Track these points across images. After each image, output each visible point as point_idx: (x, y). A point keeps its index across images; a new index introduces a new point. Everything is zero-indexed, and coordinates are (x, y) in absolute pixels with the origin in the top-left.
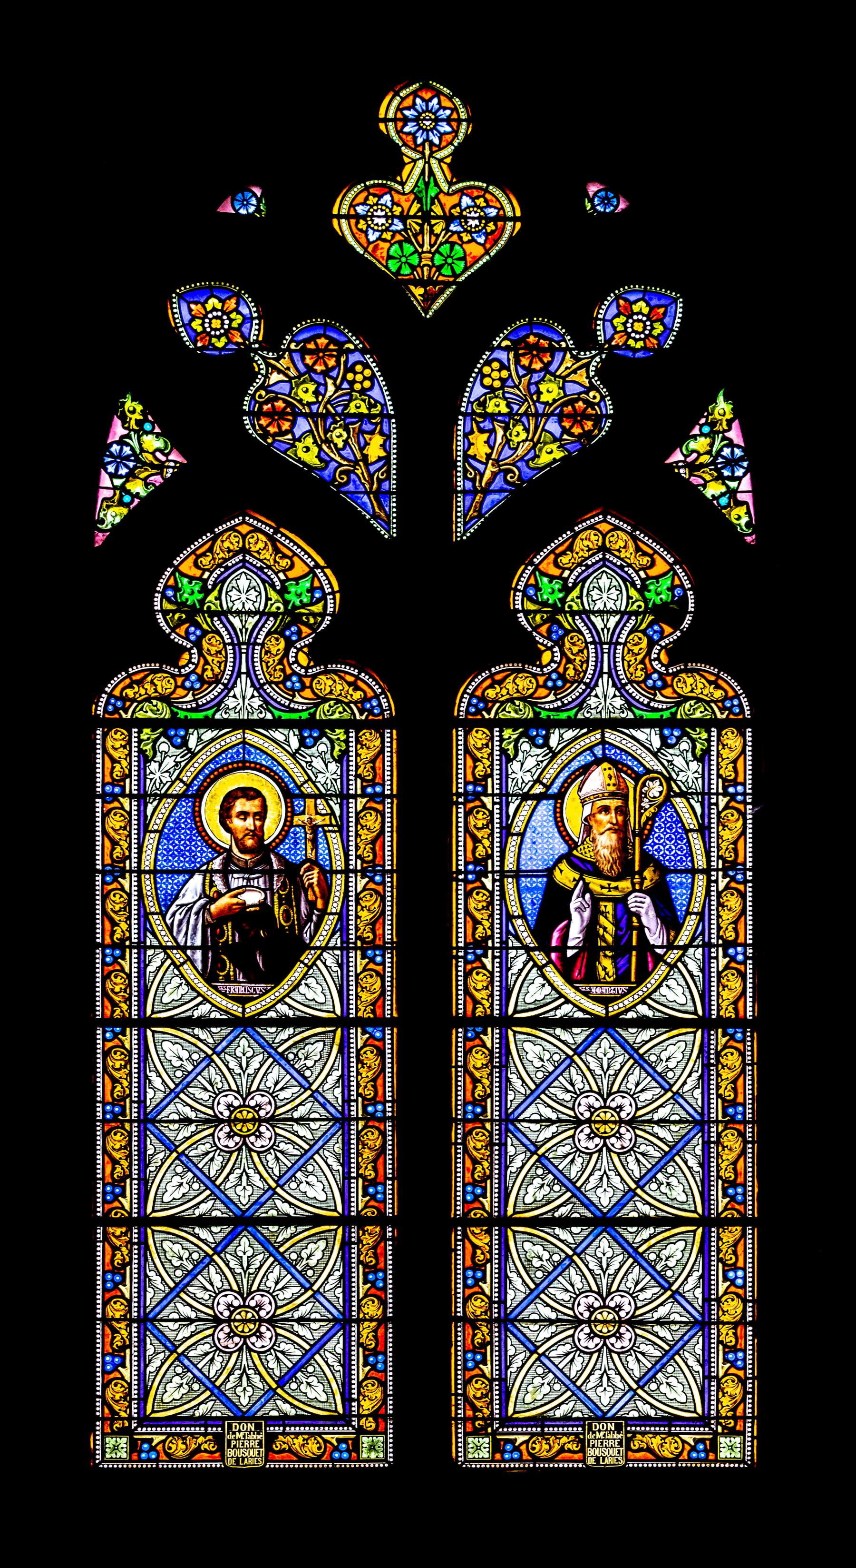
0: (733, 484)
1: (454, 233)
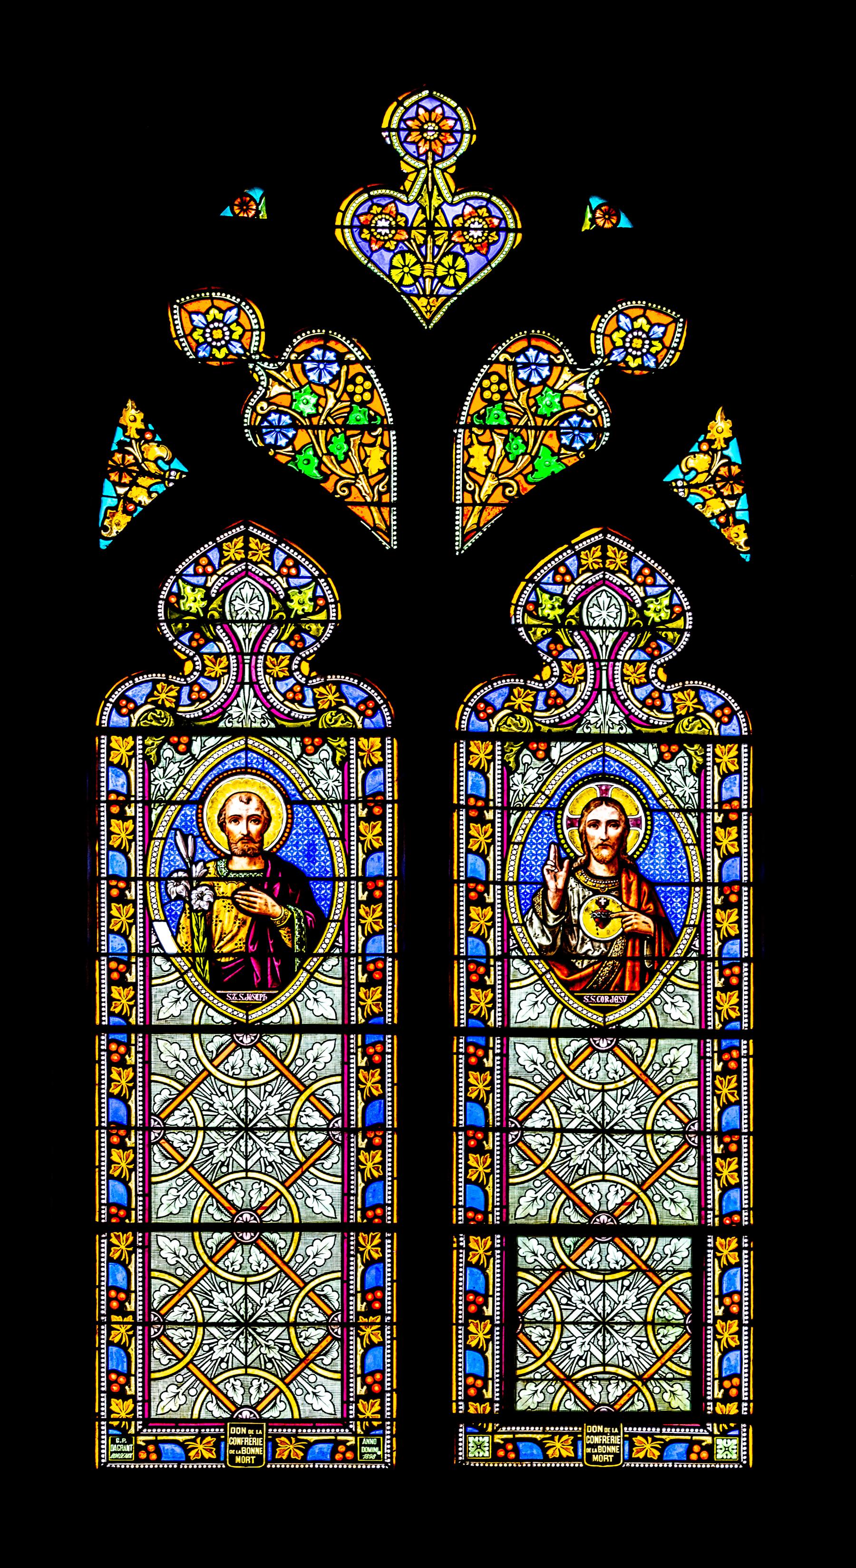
1: (456, 243)
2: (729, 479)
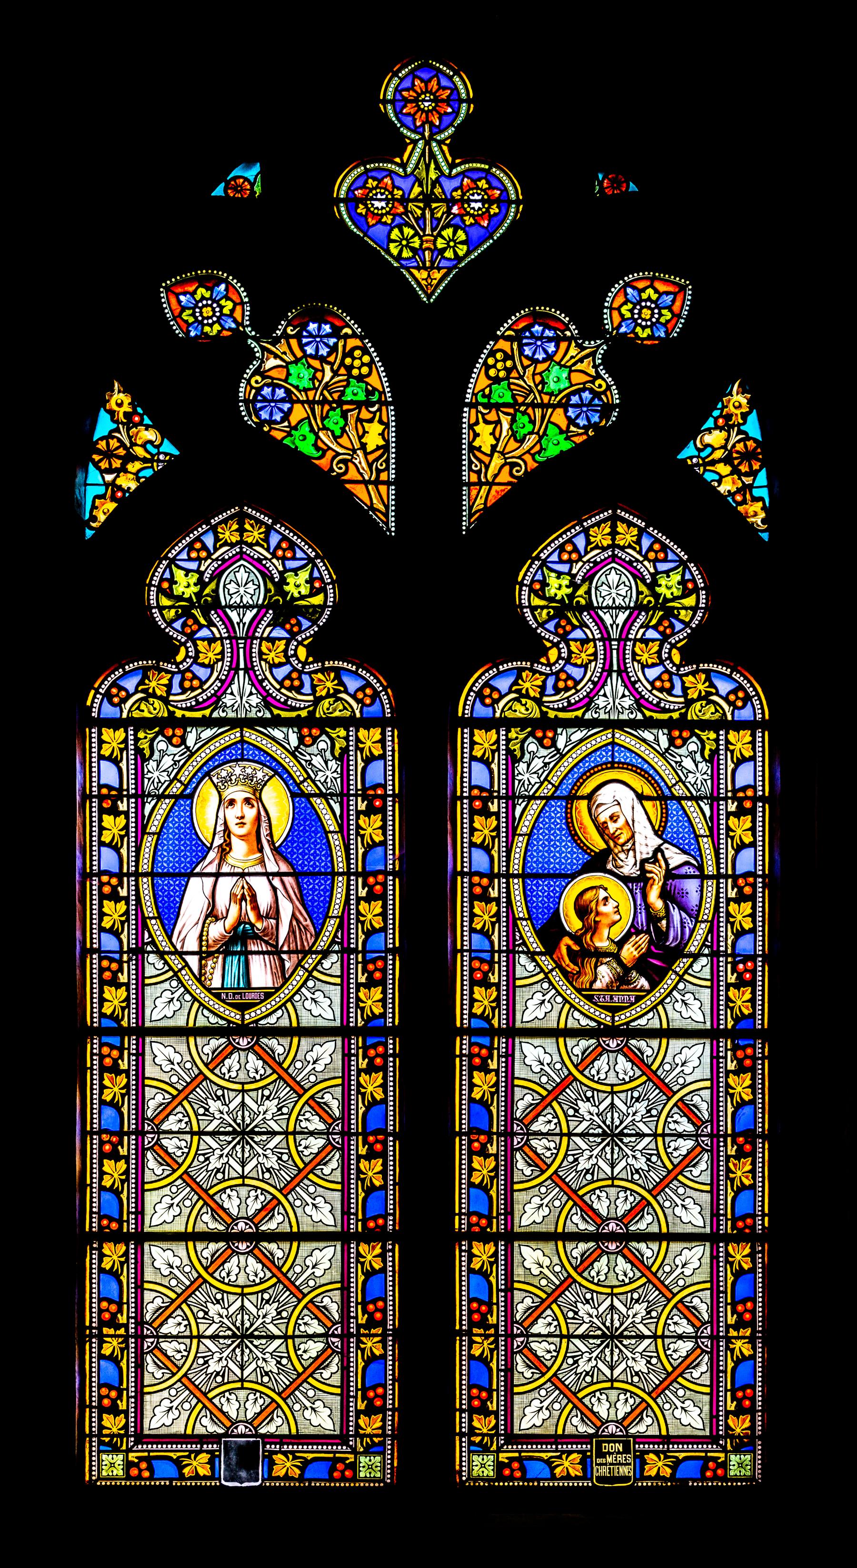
0: (748, 480)
2: (747, 456)
